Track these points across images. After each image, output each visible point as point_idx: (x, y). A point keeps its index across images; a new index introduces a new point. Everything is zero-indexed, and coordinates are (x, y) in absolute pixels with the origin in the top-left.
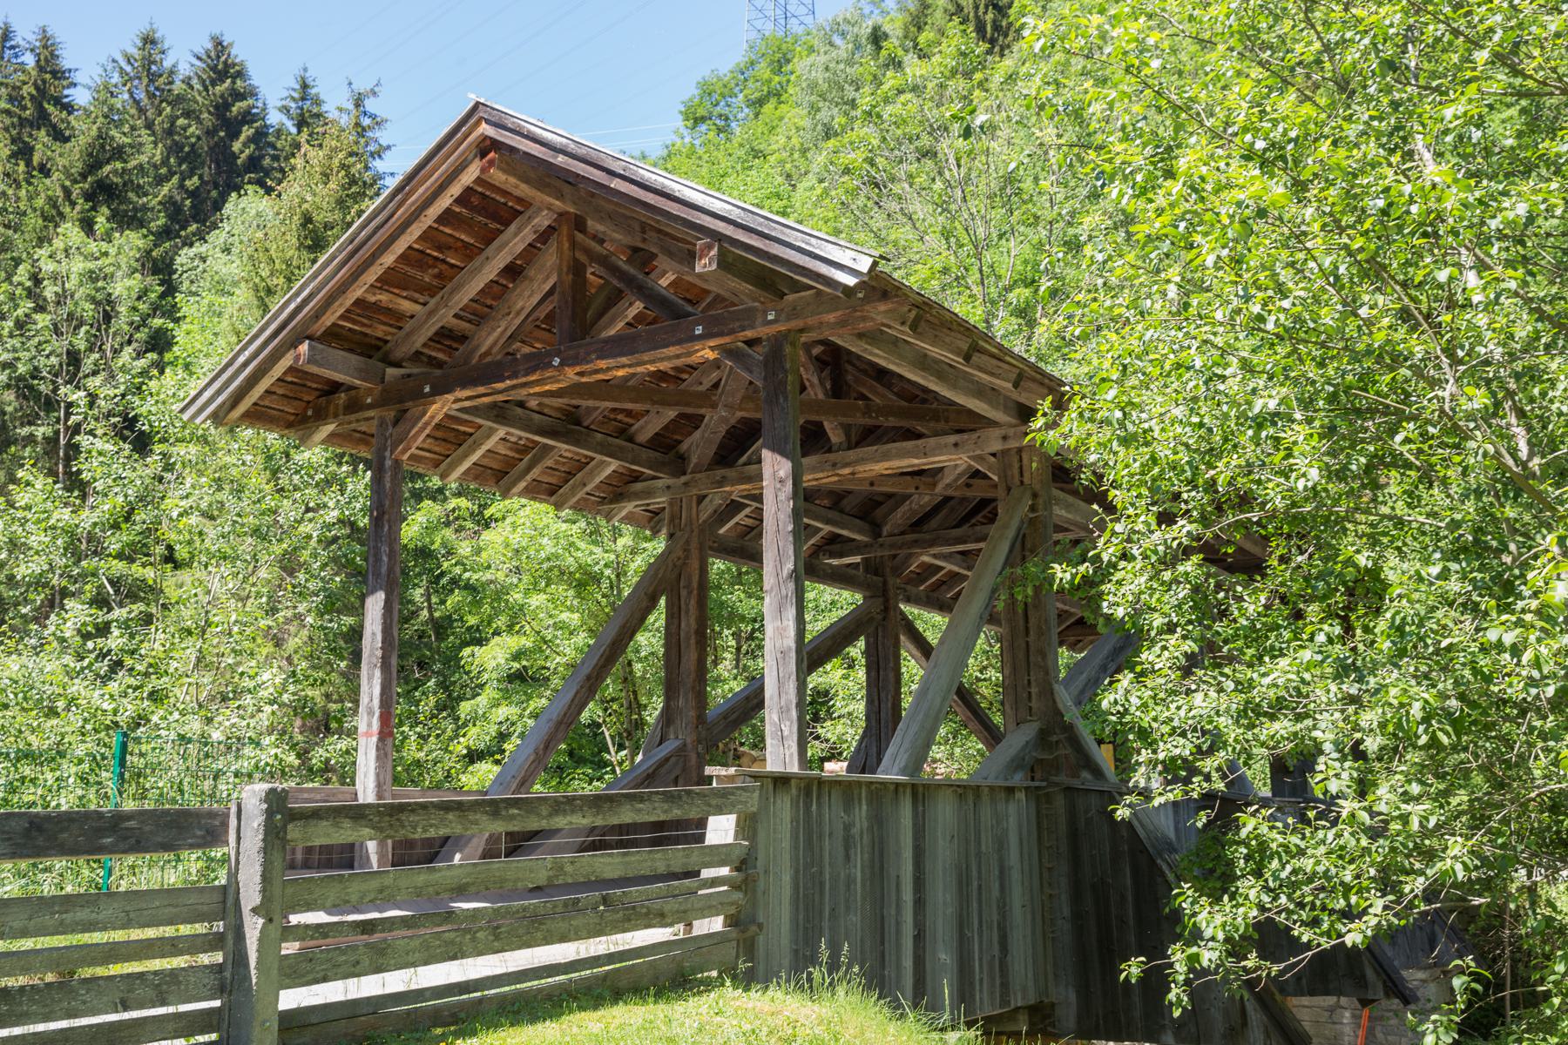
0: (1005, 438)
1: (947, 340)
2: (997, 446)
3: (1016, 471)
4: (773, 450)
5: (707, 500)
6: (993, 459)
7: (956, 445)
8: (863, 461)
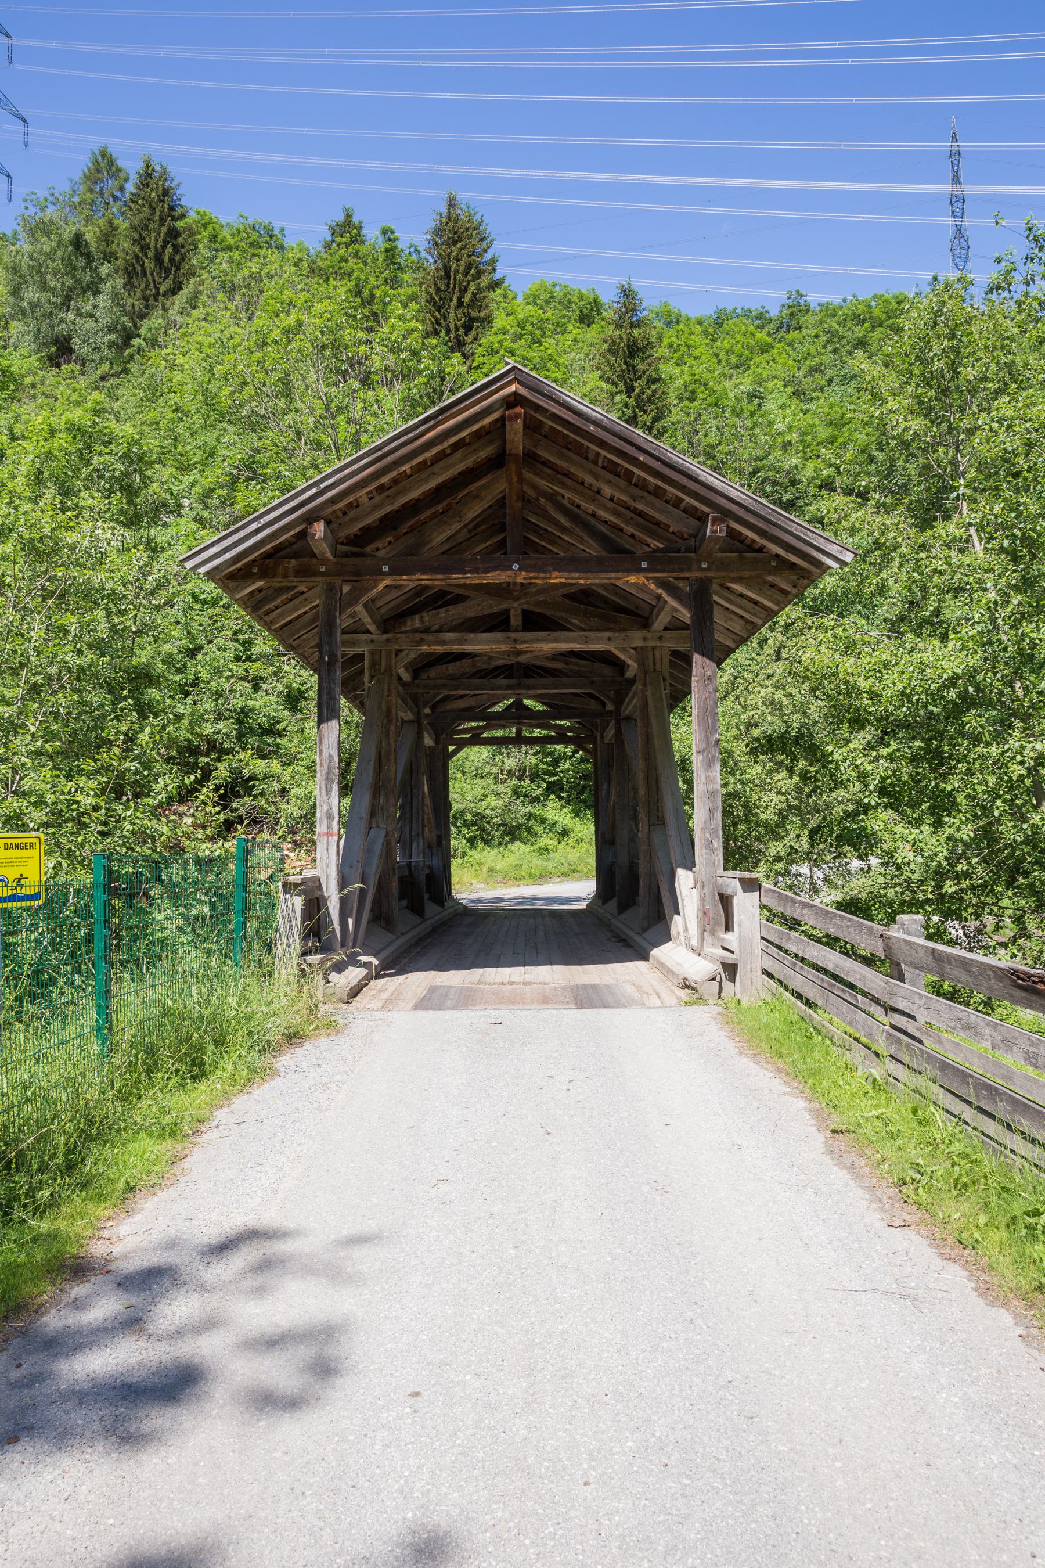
0: (645, 639)
1: (769, 593)
2: (639, 643)
3: (651, 662)
4: (703, 654)
5: (404, 653)
6: (633, 651)
7: (609, 639)
8: (537, 640)
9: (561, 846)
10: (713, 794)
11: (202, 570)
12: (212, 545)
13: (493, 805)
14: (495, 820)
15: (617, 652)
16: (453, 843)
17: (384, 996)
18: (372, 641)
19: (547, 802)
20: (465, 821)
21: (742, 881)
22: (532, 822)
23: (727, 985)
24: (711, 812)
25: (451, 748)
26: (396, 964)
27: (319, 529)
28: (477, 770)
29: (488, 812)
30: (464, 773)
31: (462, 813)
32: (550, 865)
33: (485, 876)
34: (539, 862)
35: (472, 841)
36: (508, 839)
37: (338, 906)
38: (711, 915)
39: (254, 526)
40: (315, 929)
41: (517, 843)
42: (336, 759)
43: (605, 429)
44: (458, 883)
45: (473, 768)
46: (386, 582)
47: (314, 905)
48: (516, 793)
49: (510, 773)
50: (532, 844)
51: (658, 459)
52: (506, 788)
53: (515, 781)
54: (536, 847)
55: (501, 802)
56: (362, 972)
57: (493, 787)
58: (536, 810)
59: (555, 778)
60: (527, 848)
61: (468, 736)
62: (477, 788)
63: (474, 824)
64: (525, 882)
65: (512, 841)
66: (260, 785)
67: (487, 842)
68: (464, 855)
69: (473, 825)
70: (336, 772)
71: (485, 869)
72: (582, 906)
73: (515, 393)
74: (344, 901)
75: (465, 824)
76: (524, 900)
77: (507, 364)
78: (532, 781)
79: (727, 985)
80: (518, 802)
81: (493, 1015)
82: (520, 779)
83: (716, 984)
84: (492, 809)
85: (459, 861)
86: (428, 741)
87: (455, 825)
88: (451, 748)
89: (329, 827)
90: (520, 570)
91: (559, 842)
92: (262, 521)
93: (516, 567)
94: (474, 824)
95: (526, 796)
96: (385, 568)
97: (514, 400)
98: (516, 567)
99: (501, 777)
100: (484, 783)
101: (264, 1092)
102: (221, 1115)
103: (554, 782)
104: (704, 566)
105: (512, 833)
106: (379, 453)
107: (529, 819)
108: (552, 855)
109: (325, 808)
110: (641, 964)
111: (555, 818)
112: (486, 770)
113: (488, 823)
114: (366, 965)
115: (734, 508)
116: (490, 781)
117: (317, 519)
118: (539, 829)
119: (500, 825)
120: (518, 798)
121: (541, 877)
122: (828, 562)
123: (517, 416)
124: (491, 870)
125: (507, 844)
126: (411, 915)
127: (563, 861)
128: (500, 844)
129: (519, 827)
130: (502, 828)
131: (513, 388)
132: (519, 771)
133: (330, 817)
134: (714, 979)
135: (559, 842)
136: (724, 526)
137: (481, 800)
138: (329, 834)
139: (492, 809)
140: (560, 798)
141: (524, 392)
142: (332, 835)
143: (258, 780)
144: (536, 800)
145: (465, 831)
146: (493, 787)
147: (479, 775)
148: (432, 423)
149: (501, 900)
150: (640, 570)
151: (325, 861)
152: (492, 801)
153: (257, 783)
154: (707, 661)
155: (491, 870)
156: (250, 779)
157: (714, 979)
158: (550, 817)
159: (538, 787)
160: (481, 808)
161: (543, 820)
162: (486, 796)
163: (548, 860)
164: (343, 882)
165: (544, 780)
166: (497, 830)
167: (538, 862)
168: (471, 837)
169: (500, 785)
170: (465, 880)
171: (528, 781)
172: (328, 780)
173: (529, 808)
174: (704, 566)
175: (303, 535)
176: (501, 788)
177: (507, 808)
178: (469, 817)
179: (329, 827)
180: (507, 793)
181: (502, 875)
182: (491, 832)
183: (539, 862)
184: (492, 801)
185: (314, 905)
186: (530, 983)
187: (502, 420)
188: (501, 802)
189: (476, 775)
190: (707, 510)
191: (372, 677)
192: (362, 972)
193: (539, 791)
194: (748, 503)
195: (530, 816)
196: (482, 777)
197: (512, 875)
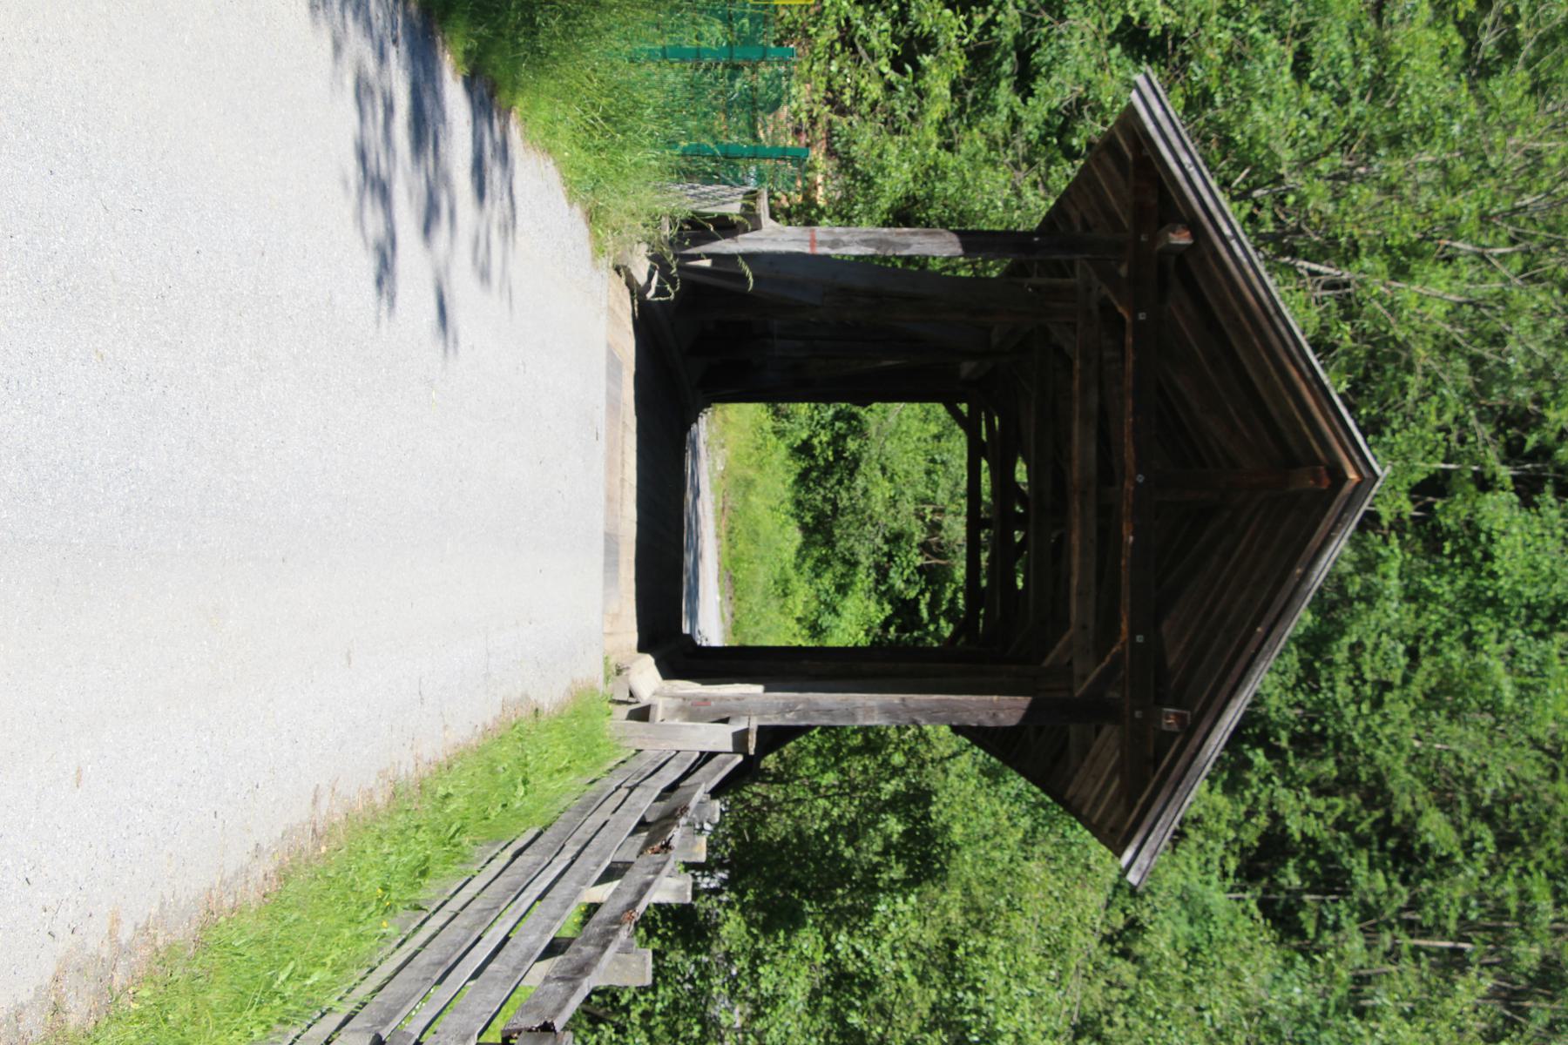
6: (1067, 660)
7: (1084, 627)
9: (792, 624)
10: (852, 715)
11: (1134, 95)
12: (1164, 108)
13: (874, 491)
14: (844, 494)
15: (1066, 638)
16: (803, 409)
17: (617, 308)
18: (1089, 290)
19: (874, 596)
20: (844, 437)
21: (746, 732)
22: (840, 568)
23: (625, 710)
24: (829, 712)
25: (964, 407)
26: (647, 321)
27: (1181, 238)
28: (943, 463)
29: (860, 482)
30: (937, 437)
31: (859, 431)
32: (755, 599)
33: (738, 472)
34: (761, 579)
35: (805, 449)
36: (808, 519)
37: (724, 251)
38: (703, 708)
39: (1186, 160)
40: (699, 228)
41: (797, 537)
42: (906, 252)
43: (1298, 585)
44: (725, 421)
45: (946, 456)
46: (1126, 316)
47: (726, 227)
48: (895, 538)
49: (935, 527)
50: (797, 567)
51: (1258, 650)
52: (906, 519)
53: (919, 537)
54: (791, 573)
55: (879, 508)
56: (641, 278)
57: (909, 492)
58: (864, 579)
59: (925, 614)
60: (789, 554)
61: (984, 437)
62: (910, 463)
63: (838, 455)
64: (725, 548)
65: (804, 528)
66: (905, 85)
67: (803, 477)
68: (780, 434)
69: (835, 452)
70: (890, 253)
71: (751, 473)
72: (686, 629)
73: (1345, 478)
74: (731, 258)
75: (837, 440)
76: (696, 536)
77: (1383, 469)
78: (921, 570)
79: (625, 710)
80: (879, 541)
81: (602, 433)
82: (925, 547)
83: (626, 697)
84: (865, 491)
85: (768, 424)
86: (967, 368)
87: (837, 416)
88: (964, 407)
89: (822, 243)
90: (1136, 484)
91: (799, 620)
92: (1192, 170)
93: (1140, 479)
94: (838, 455)
95: (890, 557)
96: (1142, 316)
97: (1339, 477)
98: (1140, 479)
99: (928, 509)
100: (918, 475)
101: (560, 192)
102: (550, 163)
103: (917, 611)
104: (1138, 714)
105: (819, 530)
106: (1272, 311)
107: (845, 561)
108: (775, 604)
109: (845, 238)
110: (633, 638)
111: (846, 614)
112: (942, 481)
113: (840, 482)
114: (648, 286)
115: (1196, 741)
116: (921, 488)
117: (1194, 235)
118: (827, 581)
119: (835, 505)
120: (887, 541)
121: (733, 580)
122: (1128, 854)
123: (1318, 481)
124: (749, 484)
125: (799, 518)
126: (705, 342)
127: (763, 625)
128: (799, 504)
129: (830, 542)
130: (828, 508)
131: (1353, 476)
132: (939, 545)
133: (835, 244)
134: (631, 695)
135: (799, 620)
136: (1175, 728)
137: (883, 469)
138: (813, 242)
139: (865, 491)
140: (886, 625)
141: (1347, 489)
142: (812, 246)
143: (915, 80)
144: (882, 573)
145: (825, 437)
146: (909, 492)
147: (914, 451)
148: (1309, 375)
149: (697, 495)
150: (1133, 634)
151: (780, 237)
152: (882, 491)
153: (909, 79)
154: (1021, 713)
155: (749, 484)
156: (917, 67)
157: (631, 695)
158: (848, 603)
159: (908, 581)
160: (869, 472)
161: (842, 589)
162: (891, 480)
163: (765, 594)
164: (750, 257)
165: (922, 592)
166: (825, 499)
167: (763, 575)
168: (813, 448)
169: (912, 508)
170: (732, 434)
171: (919, 561)
172: (880, 243)
173: (865, 561)
174: (1138, 714)
175: (1181, 220)
176: (907, 507)
177: (865, 518)
178: (852, 445)
179: (822, 243)
180: (896, 519)
181: (738, 507)
182: (823, 472)
183: (761, 579)
184: (882, 491)
185: (726, 227)
186: (623, 486)
187: (1317, 461)
188: (879, 508)
189: (933, 461)
190: (1197, 709)
191: (1037, 289)
192: (641, 278)
193: (899, 585)
194: (1202, 757)
195: (852, 564)
196: (929, 473)
197: (739, 526)
